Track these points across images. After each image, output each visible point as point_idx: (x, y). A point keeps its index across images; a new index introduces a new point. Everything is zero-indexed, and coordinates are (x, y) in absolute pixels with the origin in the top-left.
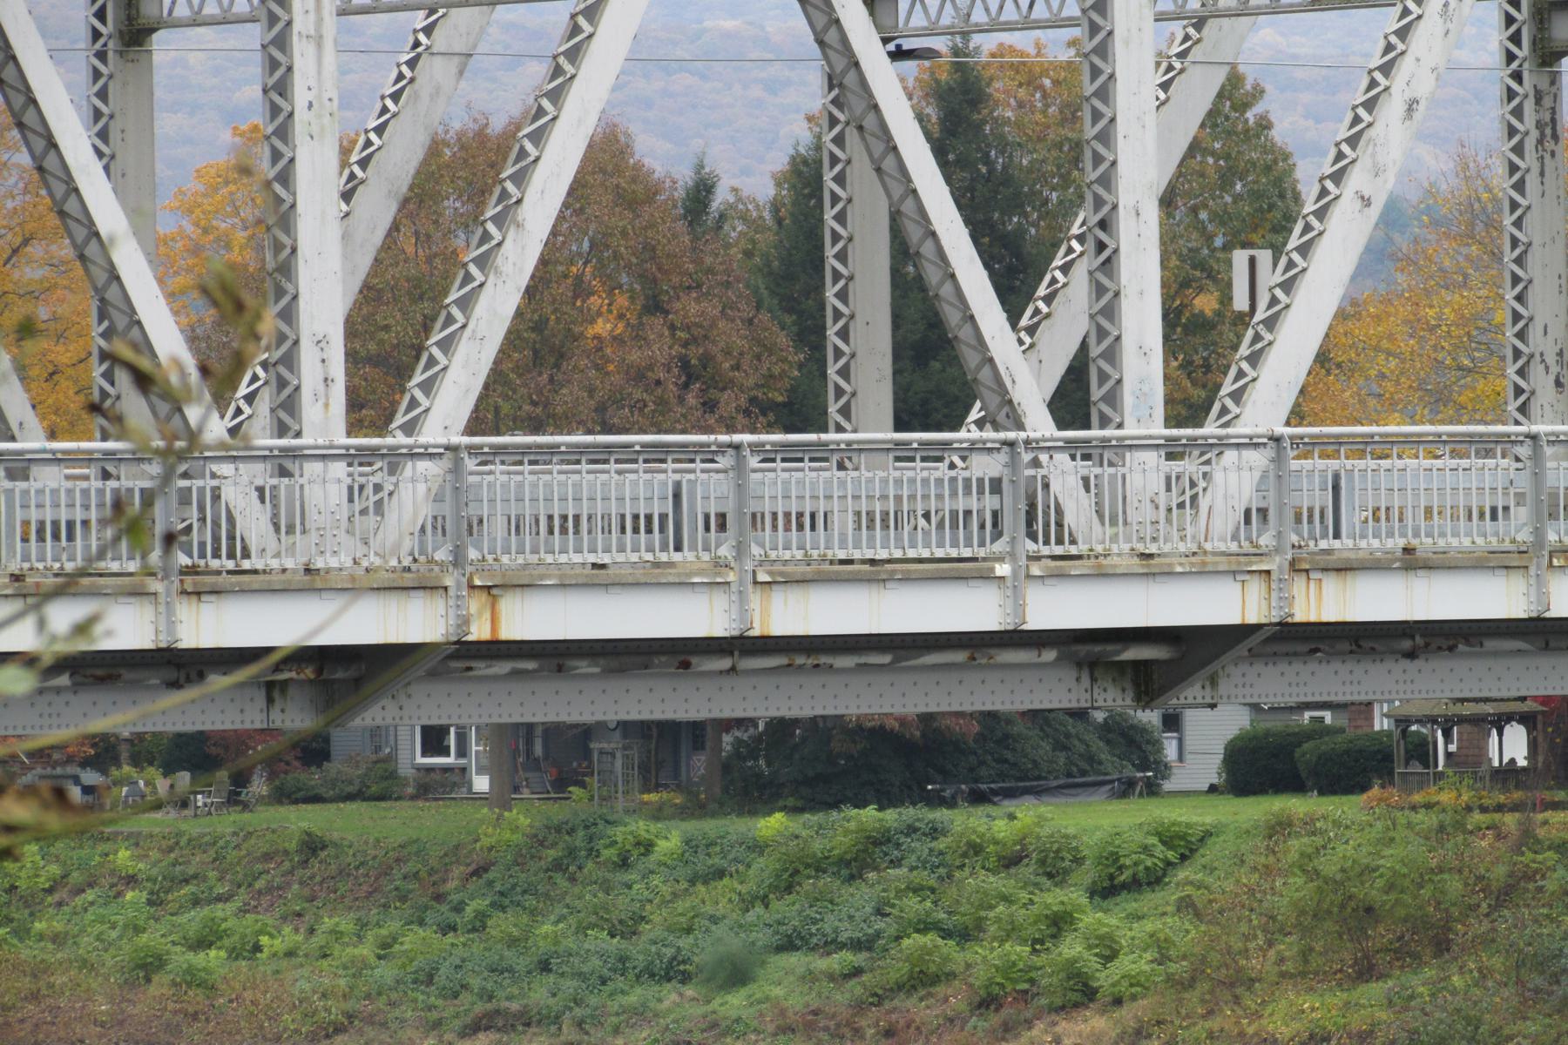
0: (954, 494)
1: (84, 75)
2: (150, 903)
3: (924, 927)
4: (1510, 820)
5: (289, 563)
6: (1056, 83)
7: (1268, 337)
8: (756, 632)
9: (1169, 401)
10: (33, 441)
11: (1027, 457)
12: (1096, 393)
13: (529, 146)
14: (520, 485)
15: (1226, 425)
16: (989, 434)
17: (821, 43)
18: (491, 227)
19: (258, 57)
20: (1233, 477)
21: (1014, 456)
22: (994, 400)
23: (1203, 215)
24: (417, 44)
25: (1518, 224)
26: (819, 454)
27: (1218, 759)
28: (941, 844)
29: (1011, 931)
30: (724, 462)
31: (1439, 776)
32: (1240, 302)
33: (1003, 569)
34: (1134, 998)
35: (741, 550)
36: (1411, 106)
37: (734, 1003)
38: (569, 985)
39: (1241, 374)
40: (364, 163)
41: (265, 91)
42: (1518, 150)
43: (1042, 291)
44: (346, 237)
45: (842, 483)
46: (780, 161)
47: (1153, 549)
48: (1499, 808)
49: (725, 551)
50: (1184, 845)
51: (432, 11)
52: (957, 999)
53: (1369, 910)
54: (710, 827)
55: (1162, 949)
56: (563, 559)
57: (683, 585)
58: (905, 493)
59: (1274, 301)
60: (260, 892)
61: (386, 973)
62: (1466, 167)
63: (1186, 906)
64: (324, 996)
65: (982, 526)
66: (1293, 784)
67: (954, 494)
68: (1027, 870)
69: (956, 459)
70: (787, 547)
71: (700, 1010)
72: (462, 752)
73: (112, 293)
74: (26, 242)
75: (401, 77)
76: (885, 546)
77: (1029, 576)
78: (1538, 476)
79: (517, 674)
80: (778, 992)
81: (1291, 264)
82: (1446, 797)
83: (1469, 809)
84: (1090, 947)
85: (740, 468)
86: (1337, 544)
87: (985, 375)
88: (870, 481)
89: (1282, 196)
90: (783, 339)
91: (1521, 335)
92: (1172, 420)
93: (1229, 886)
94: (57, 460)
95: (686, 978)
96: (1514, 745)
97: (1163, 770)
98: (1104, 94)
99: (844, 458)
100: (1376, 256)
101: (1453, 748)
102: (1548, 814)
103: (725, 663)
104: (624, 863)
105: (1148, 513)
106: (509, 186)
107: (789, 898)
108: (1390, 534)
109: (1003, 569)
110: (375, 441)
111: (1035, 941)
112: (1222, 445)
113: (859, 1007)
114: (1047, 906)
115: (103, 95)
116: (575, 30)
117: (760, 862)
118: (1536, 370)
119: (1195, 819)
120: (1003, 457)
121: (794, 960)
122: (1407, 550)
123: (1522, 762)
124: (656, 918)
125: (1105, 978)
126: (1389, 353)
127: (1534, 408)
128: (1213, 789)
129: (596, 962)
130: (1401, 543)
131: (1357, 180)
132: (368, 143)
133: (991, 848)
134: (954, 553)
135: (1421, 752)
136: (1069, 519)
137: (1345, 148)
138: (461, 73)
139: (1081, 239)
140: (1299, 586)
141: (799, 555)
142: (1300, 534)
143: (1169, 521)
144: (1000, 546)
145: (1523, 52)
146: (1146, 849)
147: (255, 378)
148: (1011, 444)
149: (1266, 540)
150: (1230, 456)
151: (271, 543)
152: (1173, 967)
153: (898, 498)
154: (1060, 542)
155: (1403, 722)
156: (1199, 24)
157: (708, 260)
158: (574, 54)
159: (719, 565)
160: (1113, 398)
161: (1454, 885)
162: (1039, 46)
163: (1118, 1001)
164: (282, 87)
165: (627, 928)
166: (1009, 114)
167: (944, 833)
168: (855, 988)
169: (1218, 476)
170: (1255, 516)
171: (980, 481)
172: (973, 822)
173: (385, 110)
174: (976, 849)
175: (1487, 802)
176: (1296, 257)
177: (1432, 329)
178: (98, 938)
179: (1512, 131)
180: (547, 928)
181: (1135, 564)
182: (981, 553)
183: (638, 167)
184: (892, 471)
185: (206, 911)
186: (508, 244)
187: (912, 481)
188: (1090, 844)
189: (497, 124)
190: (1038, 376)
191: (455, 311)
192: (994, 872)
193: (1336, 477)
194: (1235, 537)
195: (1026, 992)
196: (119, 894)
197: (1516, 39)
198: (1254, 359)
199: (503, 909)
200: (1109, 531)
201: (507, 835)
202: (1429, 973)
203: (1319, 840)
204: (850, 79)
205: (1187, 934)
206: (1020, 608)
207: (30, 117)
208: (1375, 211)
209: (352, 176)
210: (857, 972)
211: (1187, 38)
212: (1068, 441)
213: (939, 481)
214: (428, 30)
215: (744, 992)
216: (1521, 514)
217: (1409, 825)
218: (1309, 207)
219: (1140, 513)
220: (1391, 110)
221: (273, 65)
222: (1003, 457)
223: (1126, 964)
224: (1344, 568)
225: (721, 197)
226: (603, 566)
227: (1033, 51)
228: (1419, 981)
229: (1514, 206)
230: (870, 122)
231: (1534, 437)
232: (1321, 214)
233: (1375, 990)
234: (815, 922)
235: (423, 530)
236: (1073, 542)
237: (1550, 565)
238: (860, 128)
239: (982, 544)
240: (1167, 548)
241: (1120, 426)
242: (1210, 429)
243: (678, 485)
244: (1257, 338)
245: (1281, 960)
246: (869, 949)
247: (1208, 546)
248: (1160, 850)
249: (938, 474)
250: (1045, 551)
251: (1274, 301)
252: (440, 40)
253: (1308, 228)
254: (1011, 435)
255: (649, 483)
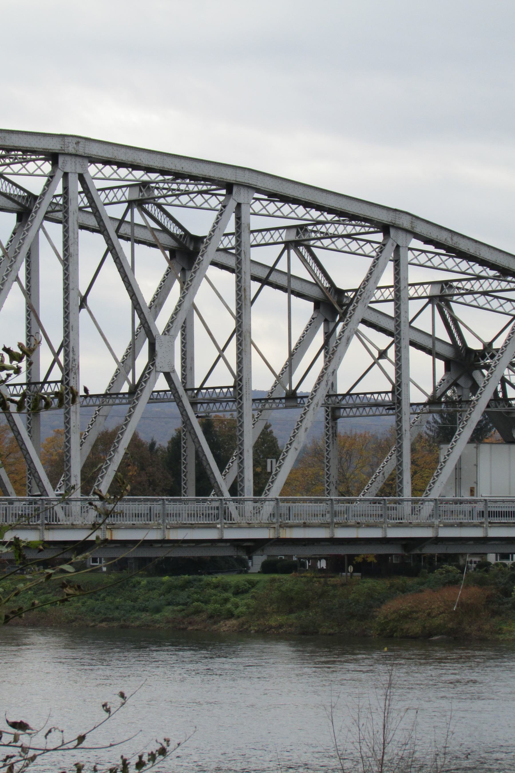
0: (209, 510)
1: (26, 419)
2: (34, 594)
3: (198, 600)
4: (322, 580)
5: (68, 523)
6: (228, 423)
7: (275, 477)
8: (167, 538)
9: (254, 491)
10: (13, 497)
11: (224, 502)
12: (239, 489)
13: (120, 435)
14: (129, 507)
15: (266, 496)
16: (216, 497)
17: (182, 414)
18: (112, 452)
19: (63, 416)
20: (268, 507)
21: (43, 502)
22: (217, 490)
23: (258, 451)
24: (96, 413)
25: (328, 454)
26: (180, 501)
27: (260, 566)
28: (202, 583)
29: (216, 602)
30: (160, 502)
31: (307, 570)
32: (269, 470)
33: (219, 526)
34: (242, 616)
35: (164, 521)
36: (306, 429)
37: (157, 616)
38: (123, 612)
39: (269, 485)
40: (84, 439)
41: (65, 423)
42: (328, 438)
43: (227, 467)
44: (81, 454)
45: (185, 507)
46: (169, 439)
47: (250, 522)
48: (320, 577)
49: (160, 521)
50: (253, 584)
51: (99, 407)
52: (204, 616)
53: (292, 598)
54: (153, 579)
55: (248, 606)
56: (126, 523)
57: (254, 527)
58: (198, 509)
59: (277, 470)
60: (57, 592)
61: (83, 609)
62: (314, 442)
63: (253, 597)
64: (71, 614)
65: (214, 516)
66: (276, 571)
67: (209, 510)
68: (219, 589)
69: (209, 502)
70: (173, 521)
71: (150, 618)
72: (100, 562)
73: (32, 465)
74: (10, 454)
75: (92, 420)
76: (194, 520)
77: (224, 528)
78: (332, 508)
79: (116, 547)
80: (166, 614)
81: (280, 462)
82: (308, 575)
83: (313, 577)
84: (233, 605)
85: (164, 504)
86: (289, 522)
87: (215, 485)
88: (191, 507)
89: (275, 447)
90: (169, 476)
91: (328, 478)
92: (255, 495)
93: (262, 593)
94: (20, 500)
95: (147, 611)
96: (323, 564)
97: (248, 568)
98: (241, 426)
99: (186, 502)
100: (299, 461)
101: (310, 564)
102: (330, 579)
103: (160, 545)
104: (134, 586)
105: (249, 514)
106: (116, 444)
107: (169, 594)
108: (301, 520)
109: (219, 526)
110: (87, 497)
111: (221, 604)
112: (265, 500)
113: (184, 617)
114: (224, 596)
115: (29, 423)
116: (130, 411)
117: (163, 587)
118: (331, 485)
119: (255, 579)
120: (219, 502)
121: (170, 607)
122: (304, 523)
123: (325, 568)
124: (141, 598)
125: (236, 612)
126: (297, 481)
127: (331, 494)
128: (259, 572)
129: (128, 607)
130: (303, 521)
131: (294, 445)
132: (86, 434)
133: (212, 584)
134: (209, 522)
135: (303, 565)
136: (233, 516)
137: (292, 438)
138: (105, 420)
139: (235, 456)
140: (281, 530)
141: (176, 522)
142: (281, 519)
143: (254, 516)
144: (218, 521)
145: (329, 418)
146: (245, 585)
147: (61, 484)
148: (221, 499)
149: (274, 520)
150: (267, 503)
151: (64, 518)
152: (250, 610)
153: (197, 511)
154: (231, 520)
155: (299, 559)
156: (261, 412)
157: (154, 459)
158: (130, 416)
159: (159, 524)
160: (242, 490)
161: (310, 593)
162: (224, 415)
163: (239, 617)
164: (68, 422)
165: (135, 600)
166: (218, 429)
167: (202, 581)
168: (183, 613)
169: (265, 507)
170: (273, 515)
171: (214, 507)
172: (208, 579)
173: (89, 427)
174: (208, 584)
175: (317, 576)
176: (281, 461)
177: (307, 476)
178: (23, 601)
179: (327, 435)
180: (118, 600)
181: (247, 525)
182: (214, 522)
183: (139, 440)
184: (196, 505)
185: (46, 595)
186: (115, 456)
187: (200, 507)
188: (233, 583)
189: (110, 430)
190: (226, 485)
191: (104, 470)
192: (213, 589)
193: (289, 507)
194: (268, 520)
195: (219, 615)
196: (28, 592)
197: (328, 415)
198: (272, 482)
199: (109, 596)
200: (241, 518)
201: (110, 580)
202: (304, 612)
203: (281, 583)
204: (188, 422)
205: (253, 603)
206: (222, 534)
207: (14, 428)
208: (298, 452)
209: (82, 441)
210: (184, 610)
211: (258, 414)
212: (233, 499)
213: (206, 507)
214: (99, 411)
215: (159, 614)
216: (328, 516)
217: (301, 581)
218: (284, 450)
219: (248, 514)
220: (302, 430)
221: (66, 418)
222: (219, 502)
223: (240, 609)
224: (291, 527)
225: (157, 446)
226: (134, 524)
227: (223, 416)
228: (303, 614)
229: (327, 450)
230: (192, 431)
231: (331, 500)
232: (287, 452)
233: (293, 615)
234: (175, 599)
235: (97, 516)
236: (234, 520)
237: (335, 527)
238: (190, 433)
239: (214, 520)
240: (253, 522)
241: (244, 496)
242: (263, 497)
243: (150, 507)
244: (273, 478)
245: (273, 609)
246: (186, 605)
247: (262, 522)
248: (248, 585)
249: (205, 506)
250: (228, 522)
251: (277, 470)
252: (101, 413)
253: (284, 455)
254: (221, 498)
255: (144, 507)
